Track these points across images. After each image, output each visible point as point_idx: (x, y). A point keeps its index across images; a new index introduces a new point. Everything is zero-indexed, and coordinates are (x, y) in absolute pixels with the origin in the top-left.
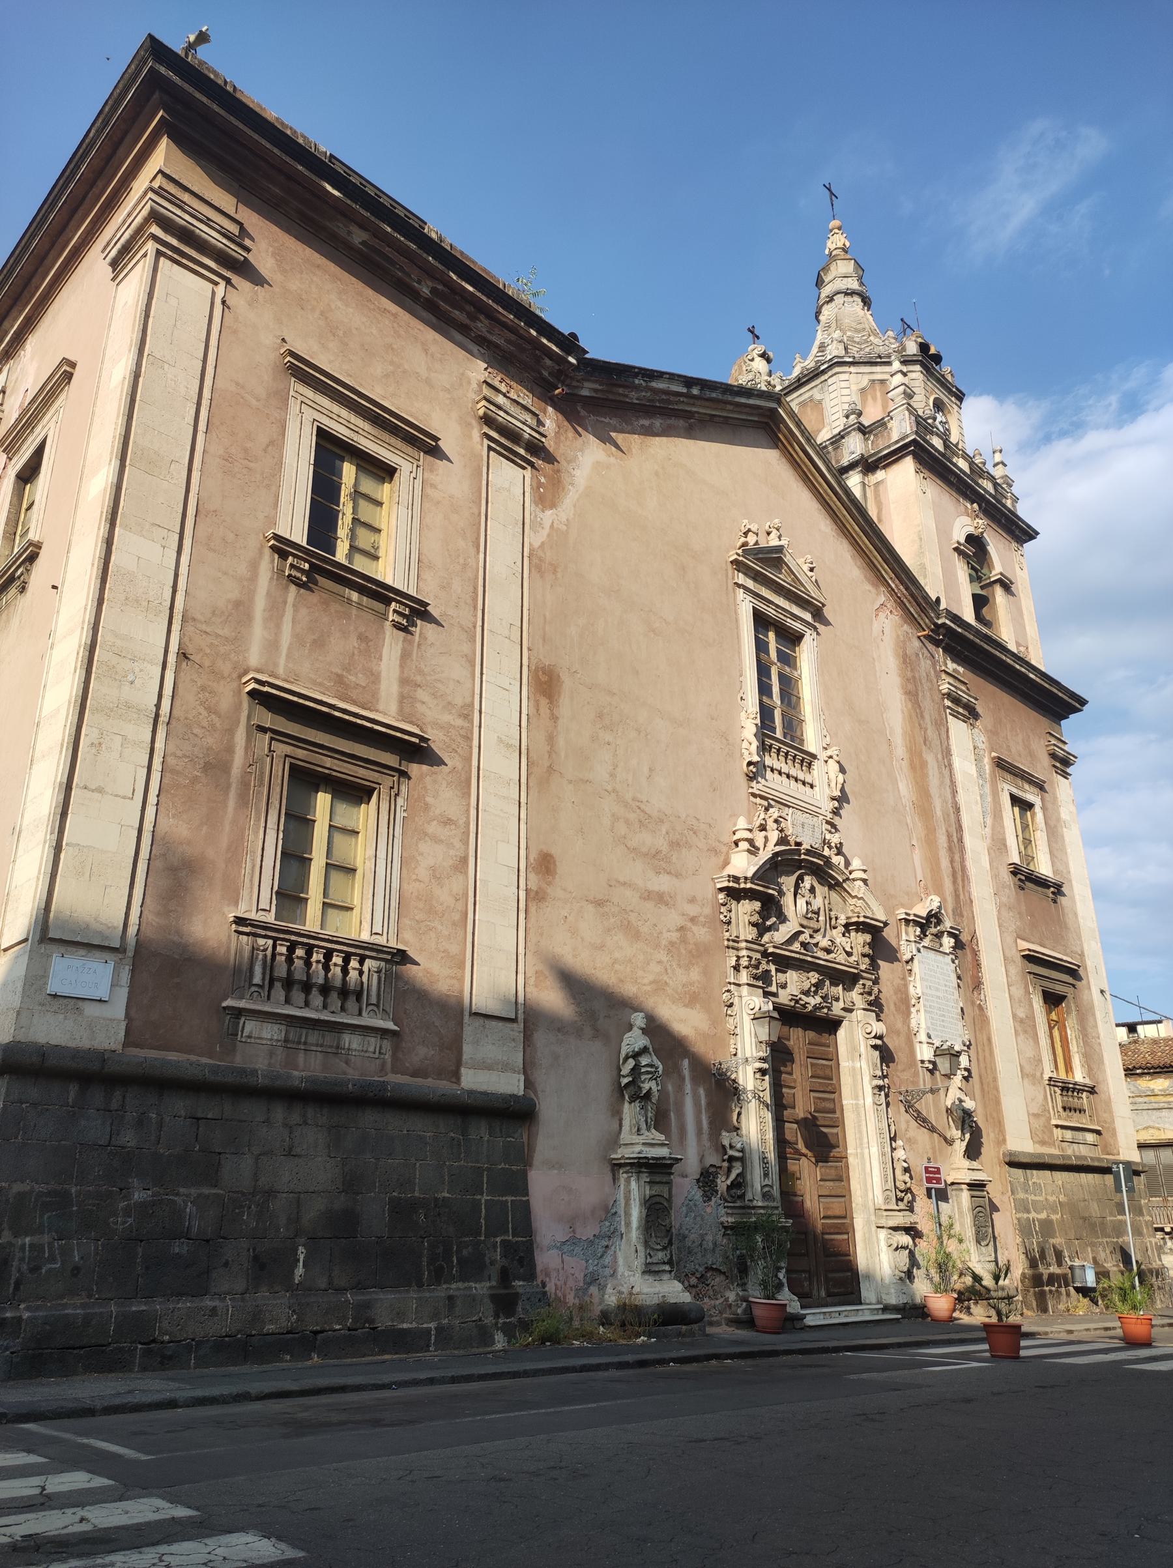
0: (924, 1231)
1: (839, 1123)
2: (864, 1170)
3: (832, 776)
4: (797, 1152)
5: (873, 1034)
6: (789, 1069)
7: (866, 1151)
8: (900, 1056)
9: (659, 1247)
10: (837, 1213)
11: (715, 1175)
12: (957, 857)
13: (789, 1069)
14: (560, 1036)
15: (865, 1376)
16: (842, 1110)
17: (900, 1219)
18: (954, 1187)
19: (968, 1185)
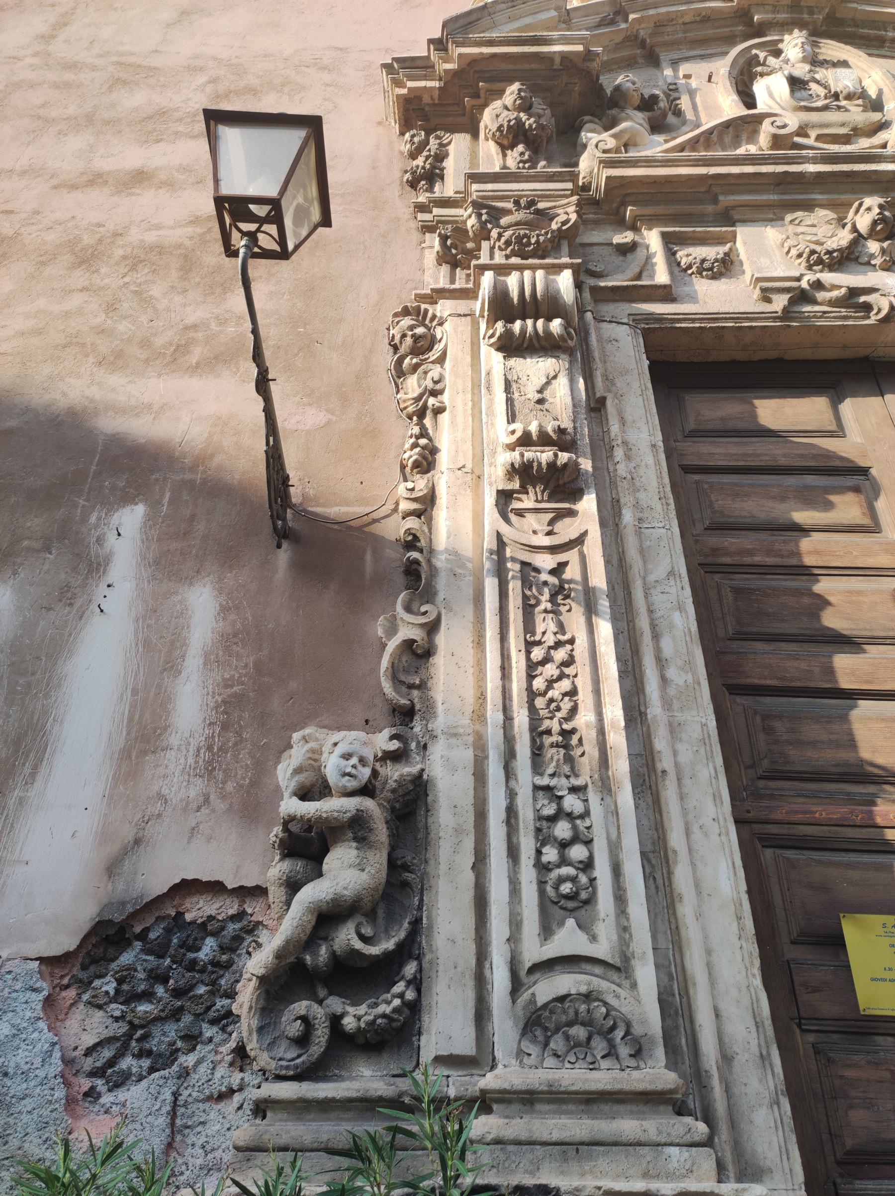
11: (240, 935)
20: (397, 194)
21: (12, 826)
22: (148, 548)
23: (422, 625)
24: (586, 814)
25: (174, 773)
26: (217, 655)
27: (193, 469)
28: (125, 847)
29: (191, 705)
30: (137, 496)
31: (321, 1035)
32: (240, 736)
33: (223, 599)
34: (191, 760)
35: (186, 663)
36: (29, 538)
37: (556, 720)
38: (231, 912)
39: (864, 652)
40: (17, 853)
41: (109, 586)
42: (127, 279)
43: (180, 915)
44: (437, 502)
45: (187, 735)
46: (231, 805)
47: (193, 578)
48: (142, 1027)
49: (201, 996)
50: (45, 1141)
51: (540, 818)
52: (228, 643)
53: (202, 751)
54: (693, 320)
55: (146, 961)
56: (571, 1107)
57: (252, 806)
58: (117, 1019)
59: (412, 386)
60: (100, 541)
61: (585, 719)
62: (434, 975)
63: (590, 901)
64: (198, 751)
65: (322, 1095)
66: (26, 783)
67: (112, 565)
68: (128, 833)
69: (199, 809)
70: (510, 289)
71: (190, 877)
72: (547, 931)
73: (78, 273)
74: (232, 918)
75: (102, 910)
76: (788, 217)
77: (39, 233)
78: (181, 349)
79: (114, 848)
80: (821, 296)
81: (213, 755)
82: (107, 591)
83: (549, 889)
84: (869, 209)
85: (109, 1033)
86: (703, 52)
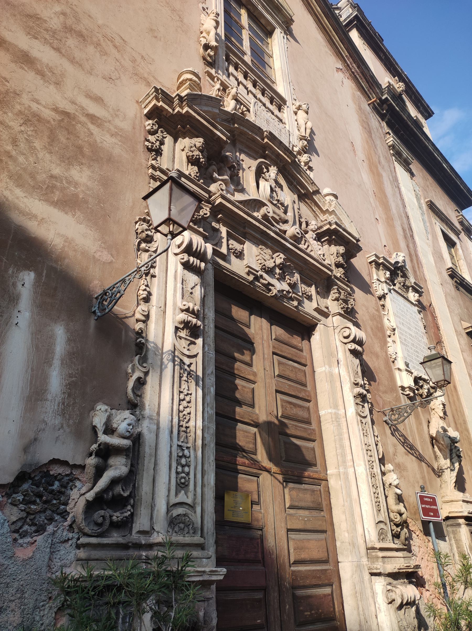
0: (426, 577)
1: (315, 437)
2: (349, 495)
3: (301, 122)
4: (255, 463)
5: (352, 338)
6: (246, 358)
7: (351, 471)
8: (380, 376)
10: (316, 555)
11: (68, 483)
12: (411, 245)
13: (246, 358)
15: (298, 176)
16: (320, 422)
17: (398, 563)
18: (450, 522)
19: (466, 518)
22: (37, 298)
23: (144, 372)
24: (189, 457)
25: (50, 411)
26: (66, 361)
29: (56, 381)
31: (108, 522)
32: (75, 400)
34: (56, 407)
35: (54, 361)
37: (184, 422)
38: (67, 473)
39: (242, 407)
41: (19, 312)
42: (22, 128)
43: (48, 471)
44: (150, 318)
45: (54, 395)
47: (56, 320)
48: (33, 514)
49: (56, 504)
50: (5, 558)
51: (178, 456)
52: (72, 356)
53: (60, 404)
54: (228, 271)
55: (32, 488)
56: (179, 548)
57: (78, 434)
58: (22, 511)
59: (144, 259)
60: (14, 285)
61: (192, 424)
62: (139, 504)
63: (187, 486)
64: (59, 404)
65: (105, 542)
68: (32, 435)
69: (59, 430)
70: (194, 244)
72: (176, 495)
74: (67, 475)
75: (22, 467)
76: (260, 247)
80: (261, 280)
81: (65, 407)
83: (178, 480)
84: (281, 258)
85: (20, 516)
86: (248, 152)
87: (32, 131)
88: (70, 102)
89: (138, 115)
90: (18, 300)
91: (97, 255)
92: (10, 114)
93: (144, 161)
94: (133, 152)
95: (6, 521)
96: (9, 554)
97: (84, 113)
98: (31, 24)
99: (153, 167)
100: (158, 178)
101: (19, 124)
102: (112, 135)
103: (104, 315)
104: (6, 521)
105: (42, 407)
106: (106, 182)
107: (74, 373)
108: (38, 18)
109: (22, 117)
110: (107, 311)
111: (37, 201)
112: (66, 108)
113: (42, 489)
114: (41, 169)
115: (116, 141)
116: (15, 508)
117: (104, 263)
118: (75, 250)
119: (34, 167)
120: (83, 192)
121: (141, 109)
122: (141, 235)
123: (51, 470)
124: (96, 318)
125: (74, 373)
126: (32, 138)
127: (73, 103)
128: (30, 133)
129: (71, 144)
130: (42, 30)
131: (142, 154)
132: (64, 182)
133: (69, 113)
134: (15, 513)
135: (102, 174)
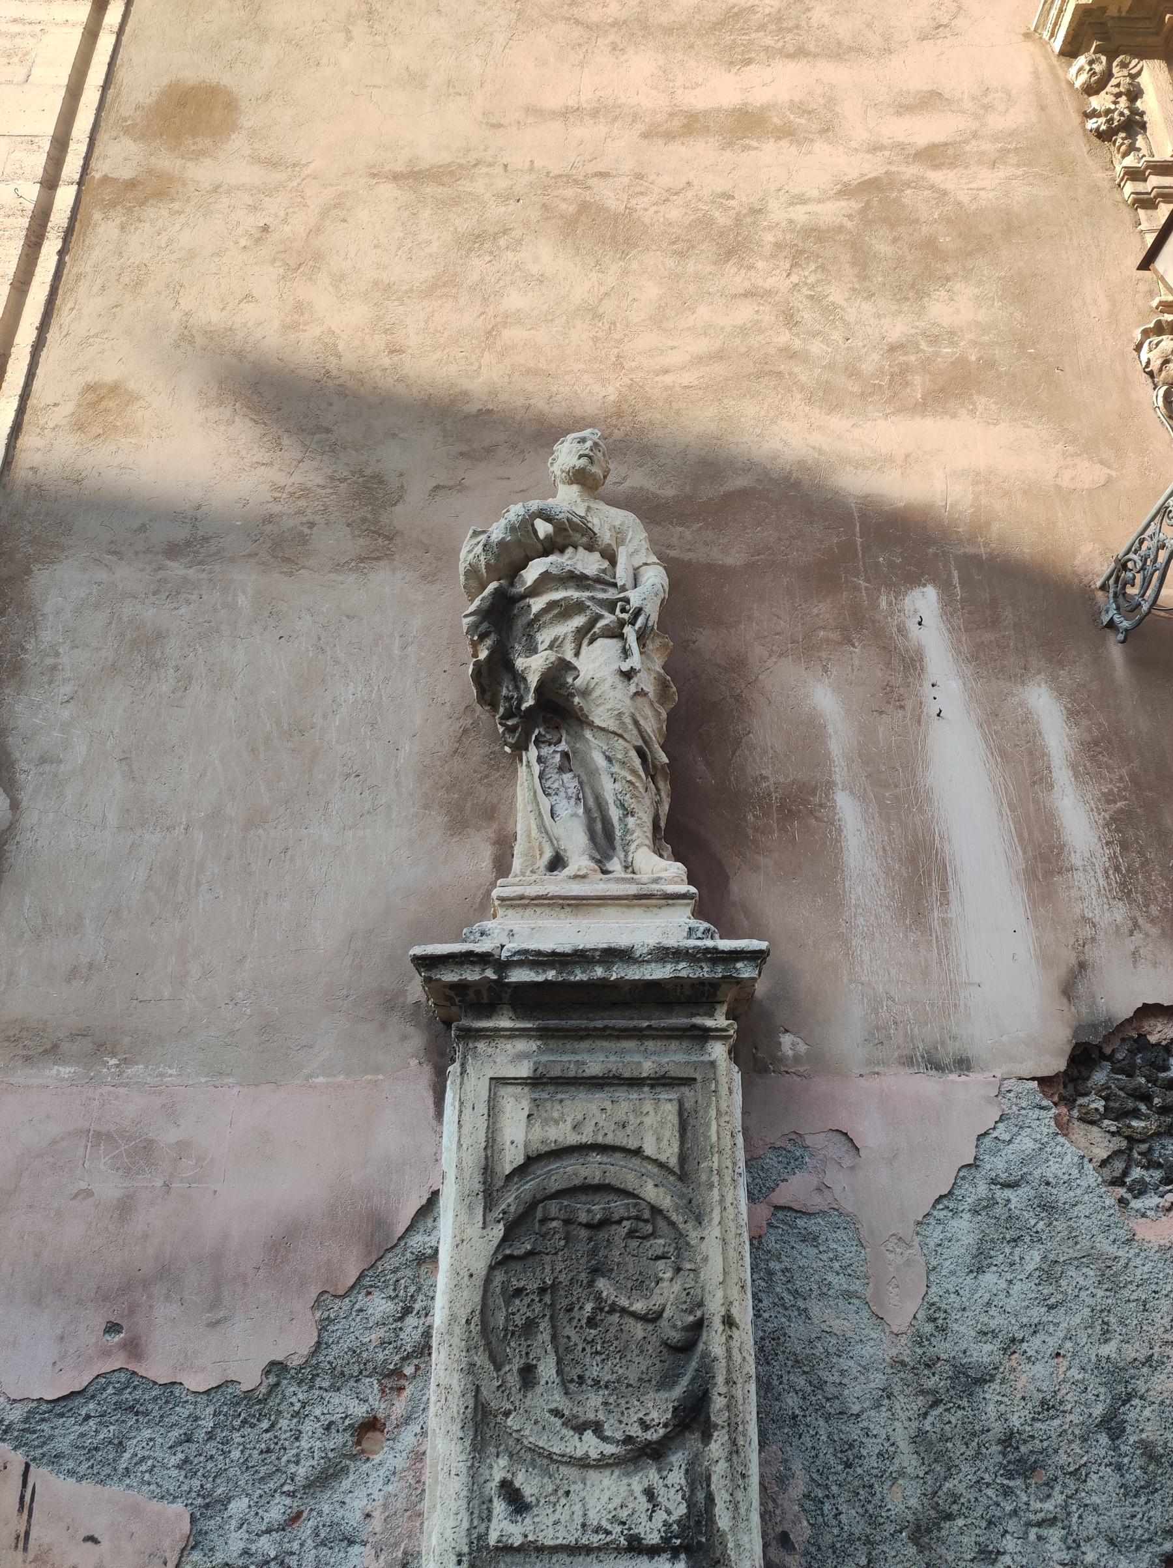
9: (590, 1445)
14: (176, 569)
20: (1085, 150)
21: (947, 948)
27: (972, 540)
28: (1072, 971)
29: (1079, 822)
30: (922, 575)
33: (1065, 700)
34: (1102, 882)
35: (1054, 775)
36: (824, 628)
40: (965, 975)
42: (794, 279)
43: (1142, 1036)
46: (1163, 929)
47: (1022, 675)
48: (1143, 1141)
52: (1096, 751)
53: (1111, 872)
55: (1118, 1079)
58: (1113, 1134)
60: (902, 630)
64: (1106, 872)
66: (941, 904)
67: (927, 660)
68: (1069, 957)
71: (1150, 1002)
73: (730, 268)
75: (1075, 1032)
77: (655, 208)
78: (901, 376)
79: (1062, 971)
81: (1124, 876)
82: (934, 692)
87: (815, 271)
88: (868, 151)
89: (1043, 66)
90: (921, 660)
91: (1065, 481)
92: (760, 264)
93: (1100, 175)
94: (1063, 171)
95: (1086, 1160)
96: (1122, 1234)
97: (908, 156)
98: (728, 39)
99: (1134, 175)
100: (1158, 195)
101: (785, 274)
102: (993, 165)
103: (1141, 620)
104: (1086, 1160)
105: (1068, 888)
106: (1019, 290)
107: (1116, 790)
108: (736, 14)
109: (784, 254)
110: (1145, 607)
111: (881, 424)
112: (866, 171)
113: (1143, 1080)
114: (864, 346)
115: (1010, 171)
116: (1095, 1129)
117: (1090, 491)
118: (1006, 494)
119: (848, 349)
120: (974, 343)
121: (1044, 45)
122: (1163, 373)
123: (1149, 1033)
124: (1121, 637)
125: (1116, 790)
126: (820, 289)
127: (876, 148)
128: (812, 279)
129: (905, 248)
130: (753, 35)
131: (1090, 162)
132: (923, 345)
133: (875, 179)
134: (1098, 1140)
135: (1003, 274)
